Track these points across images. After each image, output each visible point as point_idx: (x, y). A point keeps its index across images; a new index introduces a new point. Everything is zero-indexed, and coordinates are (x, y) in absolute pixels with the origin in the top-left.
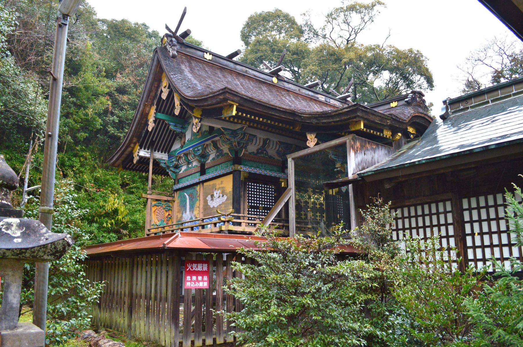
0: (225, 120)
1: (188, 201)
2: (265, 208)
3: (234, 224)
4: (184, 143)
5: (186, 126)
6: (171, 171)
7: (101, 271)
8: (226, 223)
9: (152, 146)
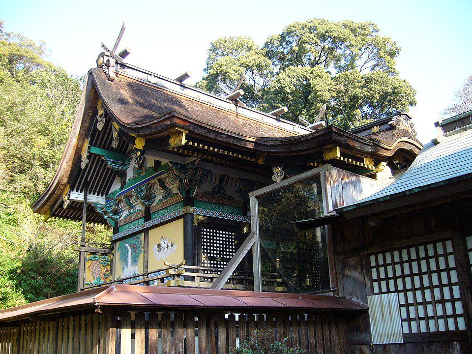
0: (172, 152)
1: (130, 253)
2: (223, 260)
3: (186, 278)
4: (125, 182)
5: (127, 162)
6: (109, 217)
7: (18, 340)
8: (176, 278)
9: (86, 188)
